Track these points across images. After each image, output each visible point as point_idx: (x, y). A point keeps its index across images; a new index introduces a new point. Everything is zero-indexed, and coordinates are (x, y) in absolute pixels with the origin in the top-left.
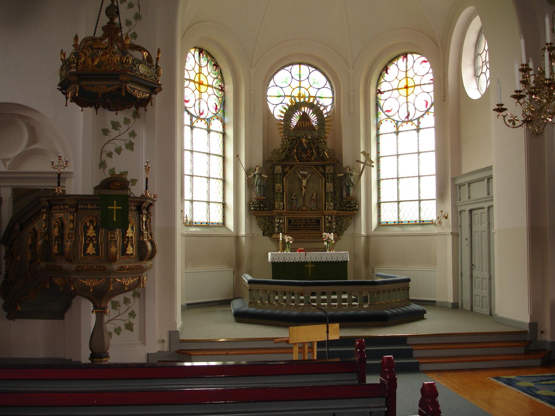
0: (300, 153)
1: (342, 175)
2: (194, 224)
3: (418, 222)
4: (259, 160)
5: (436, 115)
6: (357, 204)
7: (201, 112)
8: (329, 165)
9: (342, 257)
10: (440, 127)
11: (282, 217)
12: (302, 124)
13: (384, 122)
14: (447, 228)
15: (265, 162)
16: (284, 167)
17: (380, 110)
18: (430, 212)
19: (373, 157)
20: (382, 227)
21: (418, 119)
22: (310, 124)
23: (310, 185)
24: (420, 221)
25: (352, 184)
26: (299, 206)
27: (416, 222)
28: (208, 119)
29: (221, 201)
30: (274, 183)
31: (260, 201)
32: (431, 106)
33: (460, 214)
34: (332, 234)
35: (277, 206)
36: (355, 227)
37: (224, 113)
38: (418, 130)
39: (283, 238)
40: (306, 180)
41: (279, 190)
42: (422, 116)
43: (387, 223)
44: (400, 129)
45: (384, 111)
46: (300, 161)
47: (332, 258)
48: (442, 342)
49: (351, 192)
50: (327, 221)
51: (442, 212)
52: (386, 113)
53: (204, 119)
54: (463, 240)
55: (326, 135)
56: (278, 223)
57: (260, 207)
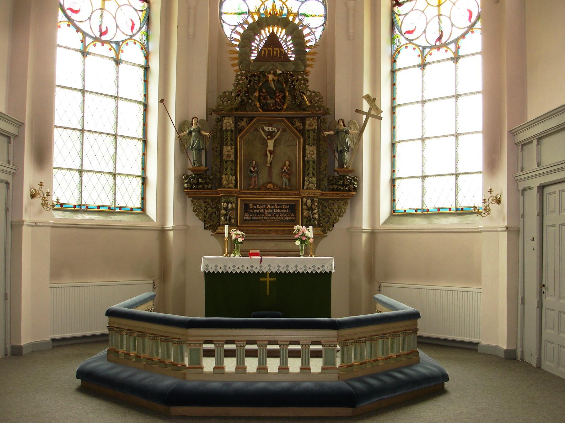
1: (332, 133)
2: (84, 208)
3: (453, 210)
4: (199, 109)
5: (484, 30)
6: (355, 180)
7: (104, 30)
9: (323, 266)
10: (492, 52)
11: (232, 199)
12: (269, 51)
13: (403, 51)
14: (499, 217)
15: (209, 112)
16: (238, 119)
17: (397, 32)
18: (473, 194)
19: (385, 104)
20: (397, 218)
21: (456, 41)
22: (281, 52)
23: (278, 148)
24: (457, 209)
26: (261, 182)
27: (450, 209)
28: (117, 43)
29: (140, 174)
30: (222, 143)
31: (198, 174)
32: (478, 17)
33: (523, 195)
34: (311, 228)
35: (224, 182)
36: (352, 217)
37: (148, 36)
38: (456, 59)
39: (229, 234)
40: (273, 141)
41: (229, 156)
42: (463, 36)
43: (405, 211)
44: (428, 59)
45: (403, 32)
46: (263, 110)
47: (279, 266)
49: (346, 160)
50: (304, 207)
51: (491, 191)
52: (407, 35)
53: (109, 42)
54: (528, 238)
55: (308, 69)
56: (225, 209)
57: (198, 184)
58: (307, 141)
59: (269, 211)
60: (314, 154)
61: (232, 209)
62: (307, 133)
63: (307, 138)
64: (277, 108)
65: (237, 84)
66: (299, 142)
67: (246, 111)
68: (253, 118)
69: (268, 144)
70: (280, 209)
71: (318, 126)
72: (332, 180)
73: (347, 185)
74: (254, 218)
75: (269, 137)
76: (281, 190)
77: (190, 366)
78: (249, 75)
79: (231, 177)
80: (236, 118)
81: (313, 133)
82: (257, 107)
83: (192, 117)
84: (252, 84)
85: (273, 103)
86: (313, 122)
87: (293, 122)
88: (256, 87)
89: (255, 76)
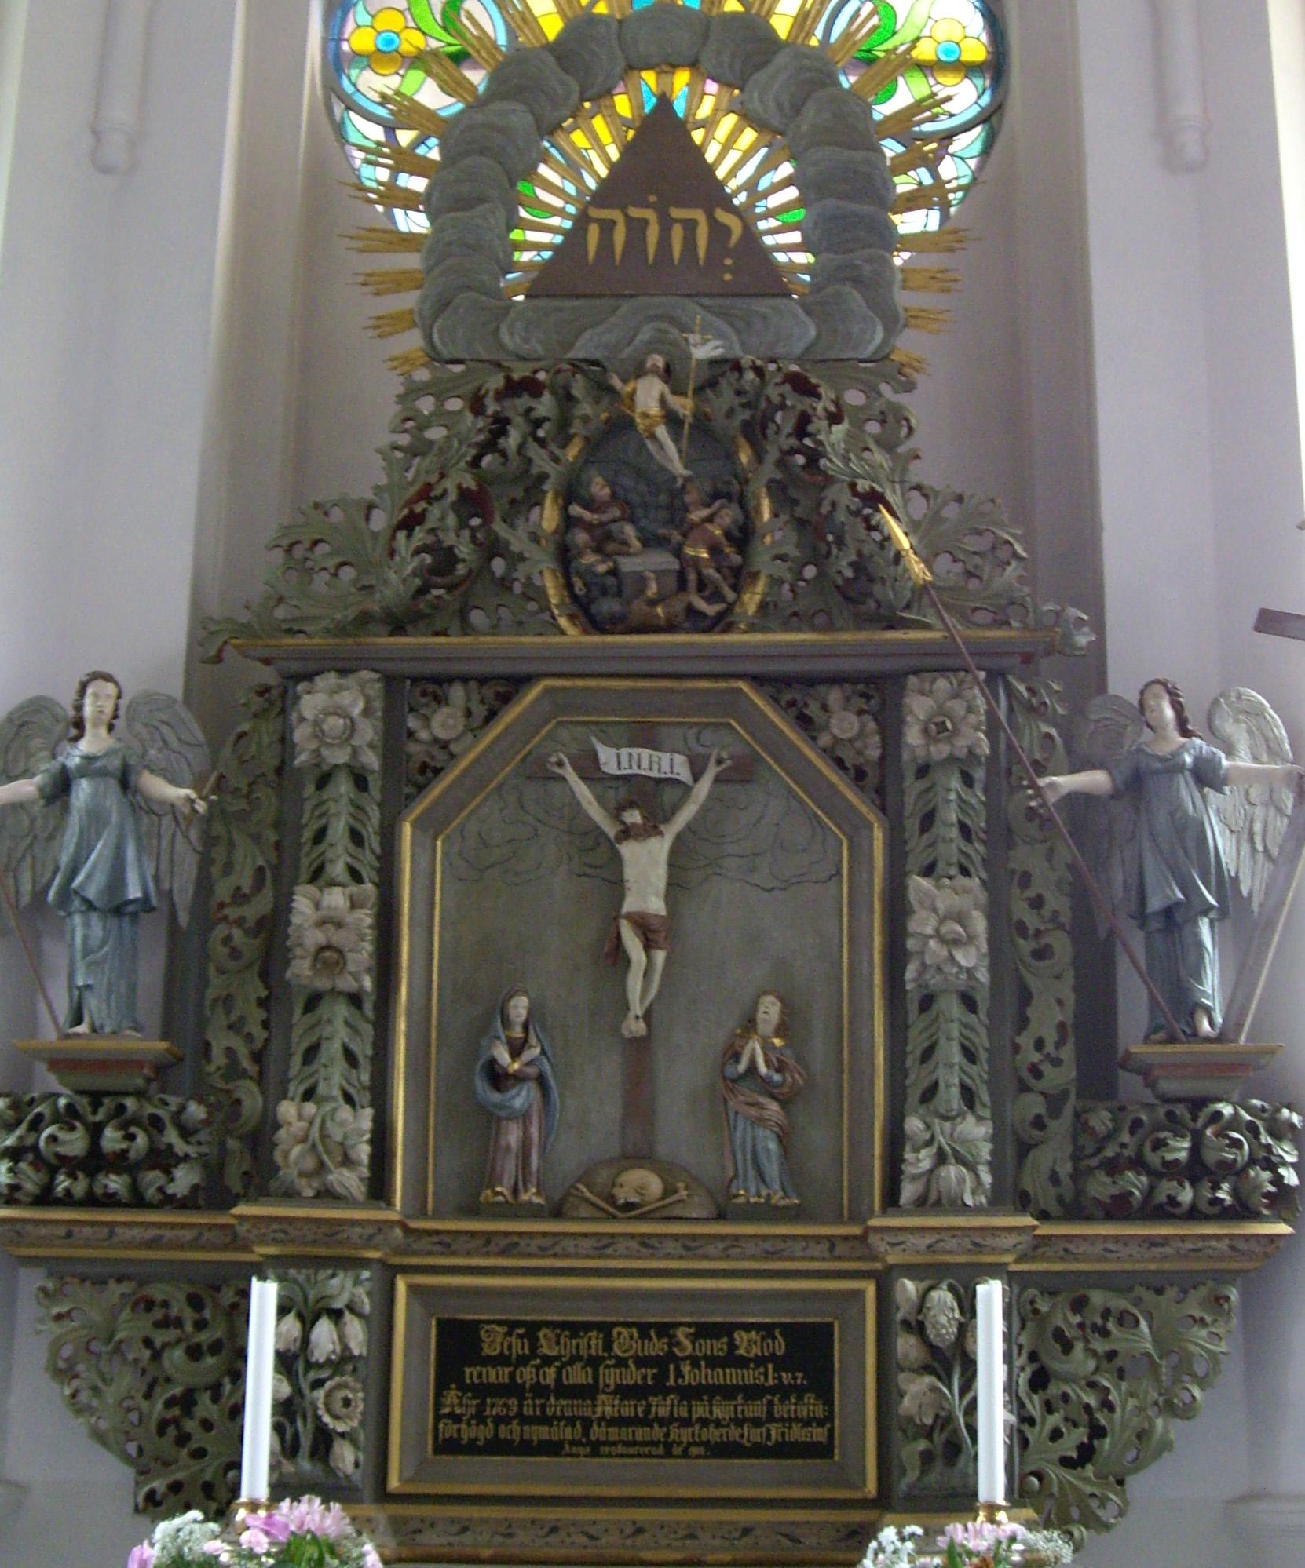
0: (604, 541)
1: (1095, 780)
8: (941, 662)
11: (341, 1287)
12: (636, 228)
15: (213, 642)
16: (409, 690)
22: (719, 231)
25: (1226, 886)
26: (570, 1155)
30: (292, 863)
35: (292, 1156)
41: (330, 957)
48: (588, 671)
49: (1212, 986)
50: (906, 1346)
58: (916, 844)
59: (633, 1376)
60: (971, 938)
61: (343, 1361)
62: (913, 788)
63: (912, 825)
64: (691, 611)
65: (413, 451)
66: (860, 855)
67: (467, 629)
68: (518, 683)
69: (630, 873)
70: (713, 1362)
71: (993, 728)
72: (1110, 1136)
73: (1228, 1169)
74: (512, 1431)
75: (634, 817)
76: (721, 1216)
77: (410, 1489)
78: (496, 382)
79: (345, 1112)
80: (391, 681)
81: (955, 783)
82: (546, 607)
83: (81, 675)
84: (512, 440)
85: (660, 574)
86: (958, 707)
87: (813, 709)
88: (541, 460)
89: (532, 387)
